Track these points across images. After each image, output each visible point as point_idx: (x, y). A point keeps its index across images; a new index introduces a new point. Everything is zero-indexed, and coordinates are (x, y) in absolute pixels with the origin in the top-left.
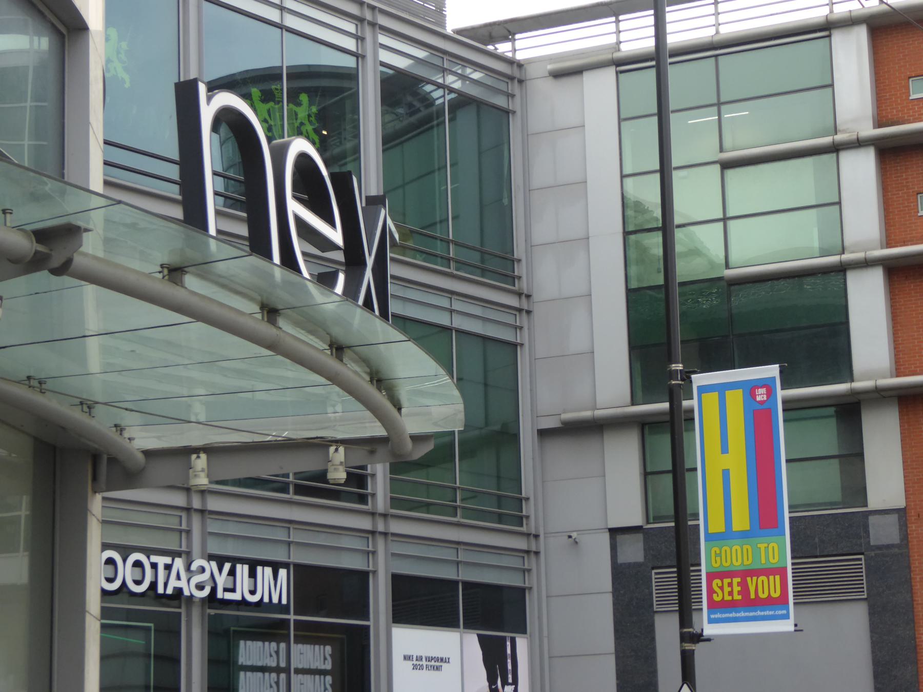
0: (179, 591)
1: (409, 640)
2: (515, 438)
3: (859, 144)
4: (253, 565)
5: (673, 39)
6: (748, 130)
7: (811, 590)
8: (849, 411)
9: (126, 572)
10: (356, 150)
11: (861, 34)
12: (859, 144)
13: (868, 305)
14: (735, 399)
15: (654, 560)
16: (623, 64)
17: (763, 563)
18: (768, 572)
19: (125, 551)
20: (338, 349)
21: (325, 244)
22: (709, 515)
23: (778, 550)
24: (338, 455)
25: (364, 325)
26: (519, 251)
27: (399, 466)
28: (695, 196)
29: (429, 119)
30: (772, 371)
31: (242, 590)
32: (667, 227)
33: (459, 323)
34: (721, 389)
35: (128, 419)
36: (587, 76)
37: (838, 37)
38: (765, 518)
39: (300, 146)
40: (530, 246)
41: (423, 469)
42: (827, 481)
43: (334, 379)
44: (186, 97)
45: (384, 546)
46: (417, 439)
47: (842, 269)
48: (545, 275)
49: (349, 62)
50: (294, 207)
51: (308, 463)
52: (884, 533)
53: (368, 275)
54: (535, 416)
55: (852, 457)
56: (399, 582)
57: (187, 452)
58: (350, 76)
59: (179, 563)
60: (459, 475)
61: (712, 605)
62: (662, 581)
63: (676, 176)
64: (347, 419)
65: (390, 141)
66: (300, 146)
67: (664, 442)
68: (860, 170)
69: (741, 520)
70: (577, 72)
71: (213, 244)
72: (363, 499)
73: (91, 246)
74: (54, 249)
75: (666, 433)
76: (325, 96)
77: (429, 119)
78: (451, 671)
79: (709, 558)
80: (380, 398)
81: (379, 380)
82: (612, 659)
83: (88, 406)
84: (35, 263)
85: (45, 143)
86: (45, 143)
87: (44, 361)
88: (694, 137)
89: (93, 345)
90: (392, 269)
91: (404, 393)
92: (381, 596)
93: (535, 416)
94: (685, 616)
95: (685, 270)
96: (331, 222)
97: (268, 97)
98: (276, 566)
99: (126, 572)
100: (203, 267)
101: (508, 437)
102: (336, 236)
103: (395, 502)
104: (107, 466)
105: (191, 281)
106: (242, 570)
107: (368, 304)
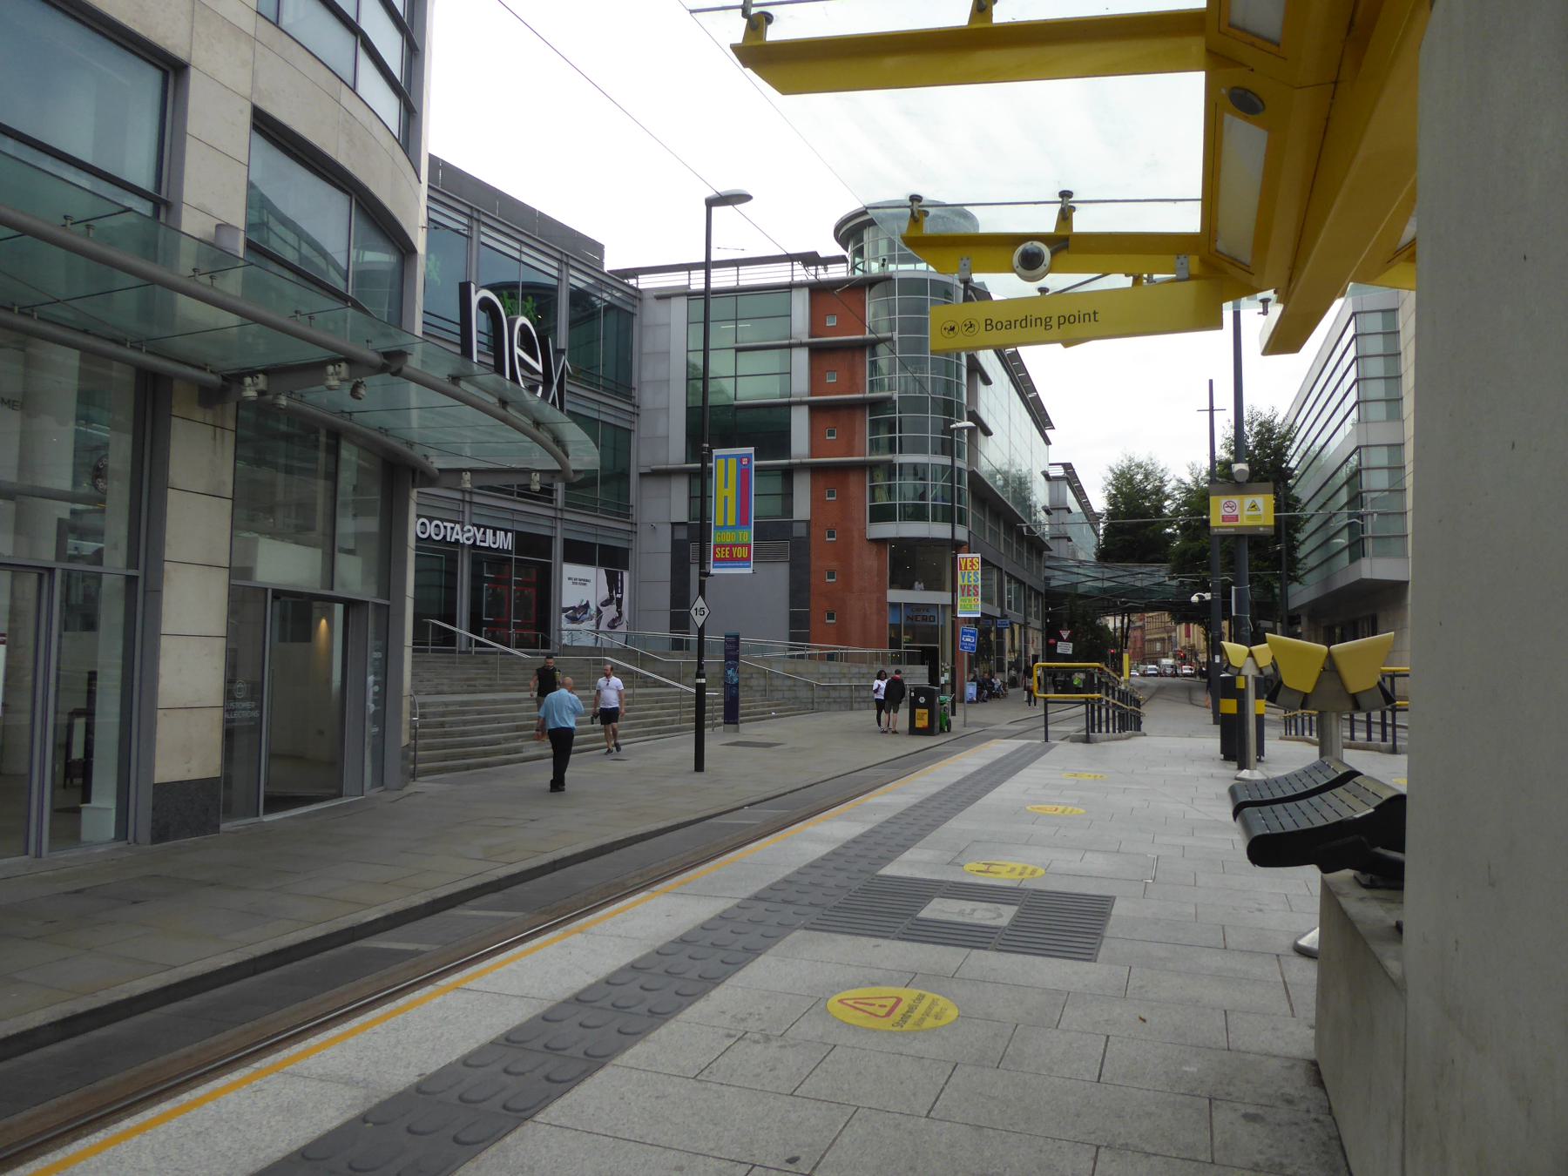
0: (457, 541)
1: (571, 571)
2: (628, 476)
3: (801, 345)
4: (495, 530)
5: (713, 286)
6: (750, 333)
7: (761, 557)
8: (788, 473)
9: (431, 530)
10: (555, 327)
11: (806, 291)
12: (801, 345)
13: (800, 422)
14: (733, 463)
15: (691, 539)
16: (690, 295)
17: (740, 541)
18: (742, 546)
19: (431, 519)
20: (537, 424)
21: (533, 371)
22: (717, 518)
23: (748, 535)
24: (536, 477)
25: (551, 413)
26: (635, 384)
27: (569, 486)
28: (721, 364)
29: (593, 314)
30: (751, 450)
31: (489, 542)
32: (705, 378)
33: (603, 417)
34: (726, 457)
35: (431, 452)
36: (673, 300)
37: (794, 292)
38: (743, 520)
39: (522, 320)
40: (640, 382)
41: (580, 486)
42: (774, 505)
43: (535, 439)
44: (465, 291)
45: (559, 523)
46: (576, 472)
47: (789, 405)
48: (648, 397)
49: (554, 282)
50: (518, 351)
51: (522, 480)
52: (800, 531)
53: (555, 388)
54: (638, 466)
55: (788, 495)
56: (567, 542)
57: (460, 471)
58: (554, 289)
59: (458, 527)
60: (599, 492)
61: (716, 560)
62: (694, 548)
63: (711, 353)
64: (542, 460)
65: (573, 324)
66: (522, 320)
67: (697, 482)
68: (801, 358)
69: (731, 521)
70: (668, 297)
71: (475, 367)
72: (551, 501)
73: (414, 363)
74: (392, 362)
75: (700, 479)
76: (540, 298)
77: (593, 314)
78: (591, 586)
79: (715, 538)
80: (558, 450)
81: (558, 441)
82: (166, 627)
83: (410, 444)
84: (383, 369)
85: (1380, 850)
86: (1380, 850)
87: (389, 420)
88: (723, 334)
89: (414, 414)
90: (567, 387)
91: (570, 449)
92: (558, 549)
93: (638, 466)
94: (703, 563)
95: (713, 400)
96: (536, 360)
97: (512, 296)
98: (507, 532)
99: (431, 530)
100: (469, 378)
101: (624, 476)
102: (539, 368)
103: (567, 504)
104: (420, 475)
105: (463, 384)
106: (489, 532)
107: (553, 403)
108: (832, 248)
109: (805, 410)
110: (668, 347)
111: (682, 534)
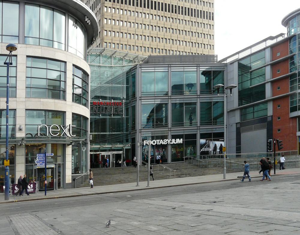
13: (268, 88)
70: (233, 63)
96: (290, 68)
108: (284, 30)
109: (270, 84)
110: (233, 78)
111: (239, 126)
